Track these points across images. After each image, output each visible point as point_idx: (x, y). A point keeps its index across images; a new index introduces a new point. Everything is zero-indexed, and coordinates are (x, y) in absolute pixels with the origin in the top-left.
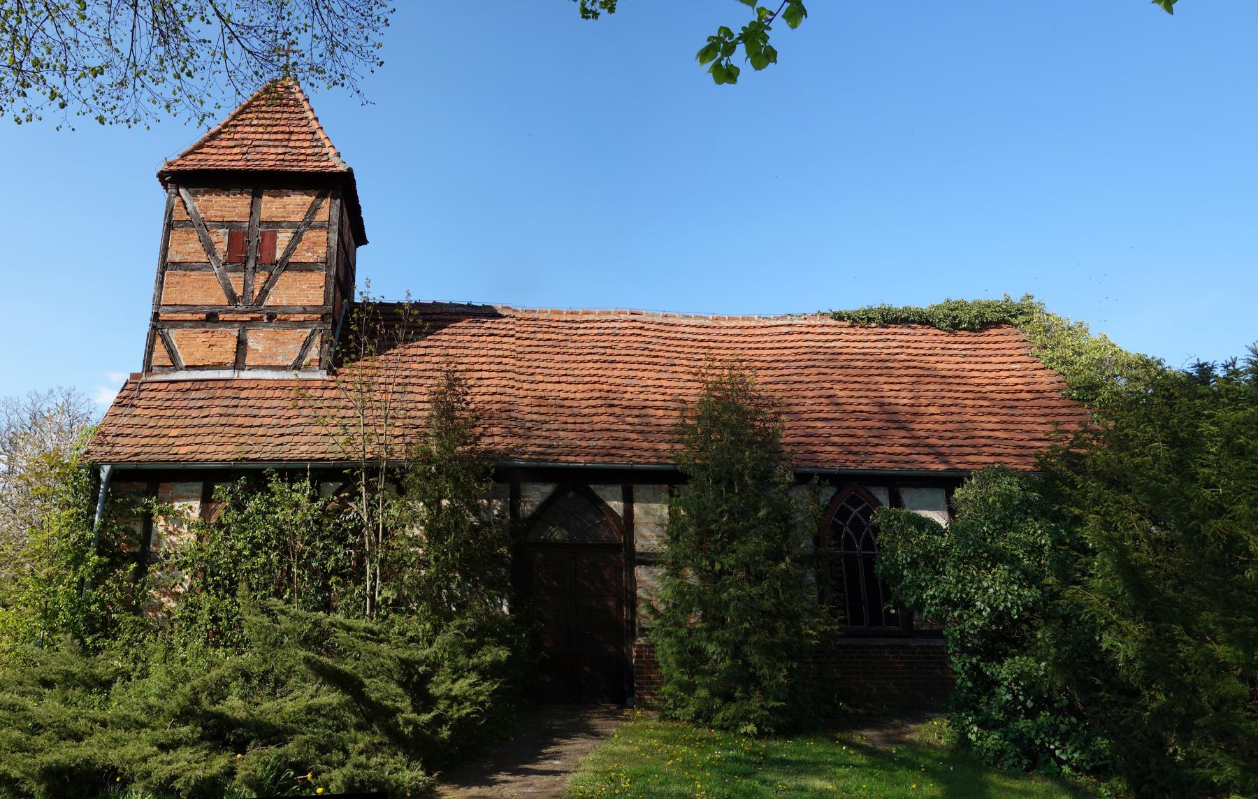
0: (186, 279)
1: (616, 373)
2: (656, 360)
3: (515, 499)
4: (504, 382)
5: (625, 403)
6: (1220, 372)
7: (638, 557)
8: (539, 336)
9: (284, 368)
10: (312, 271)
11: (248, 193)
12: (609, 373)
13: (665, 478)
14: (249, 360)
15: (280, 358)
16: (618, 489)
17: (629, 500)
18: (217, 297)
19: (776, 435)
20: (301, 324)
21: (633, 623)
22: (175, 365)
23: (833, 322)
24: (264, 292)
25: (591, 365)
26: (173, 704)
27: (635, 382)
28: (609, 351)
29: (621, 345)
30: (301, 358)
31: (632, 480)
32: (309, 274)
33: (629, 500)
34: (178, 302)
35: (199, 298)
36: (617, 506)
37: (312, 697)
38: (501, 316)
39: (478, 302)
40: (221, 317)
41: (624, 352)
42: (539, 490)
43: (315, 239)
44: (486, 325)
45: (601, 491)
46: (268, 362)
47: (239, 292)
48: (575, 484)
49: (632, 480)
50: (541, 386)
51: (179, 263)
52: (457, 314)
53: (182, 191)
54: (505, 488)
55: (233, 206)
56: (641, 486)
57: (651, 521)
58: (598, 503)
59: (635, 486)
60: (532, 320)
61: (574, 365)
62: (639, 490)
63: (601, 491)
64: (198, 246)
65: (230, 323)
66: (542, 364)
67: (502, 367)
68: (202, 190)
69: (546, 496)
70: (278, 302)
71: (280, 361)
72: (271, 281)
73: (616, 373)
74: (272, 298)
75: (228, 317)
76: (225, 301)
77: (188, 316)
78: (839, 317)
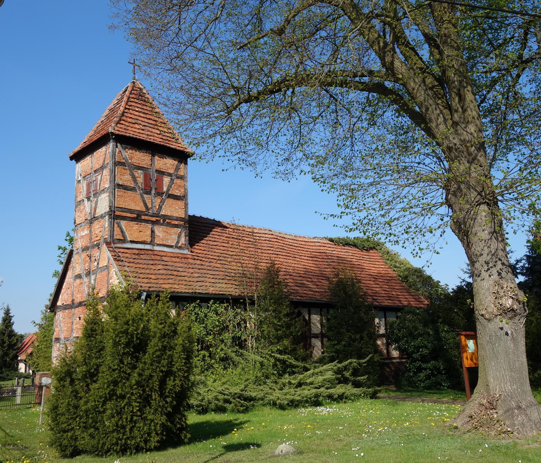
0: (126, 194)
6: (268, 174)
9: (171, 247)
10: (179, 200)
11: (149, 153)
14: (157, 241)
15: (169, 241)
16: (307, 309)
18: (140, 207)
19: (112, 296)
20: (176, 226)
22: (124, 241)
23: (330, 242)
24: (160, 207)
30: (178, 242)
32: (178, 201)
34: (124, 207)
35: (133, 207)
37: (242, 391)
38: (227, 228)
40: (143, 217)
43: (179, 184)
46: (165, 243)
47: (150, 206)
51: (121, 185)
53: (118, 145)
55: (141, 158)
60: (237, 229)
62: (313, 310)
64: (129, 177)
65: (147, 221)
68: (129, 147)
70: (166, 213)
71: (169, 243)
72: (163, 202)
74: (164, 211)
75: (146, 218)
76: (144, 209)
77: (129, 215)
78: (331, 240)
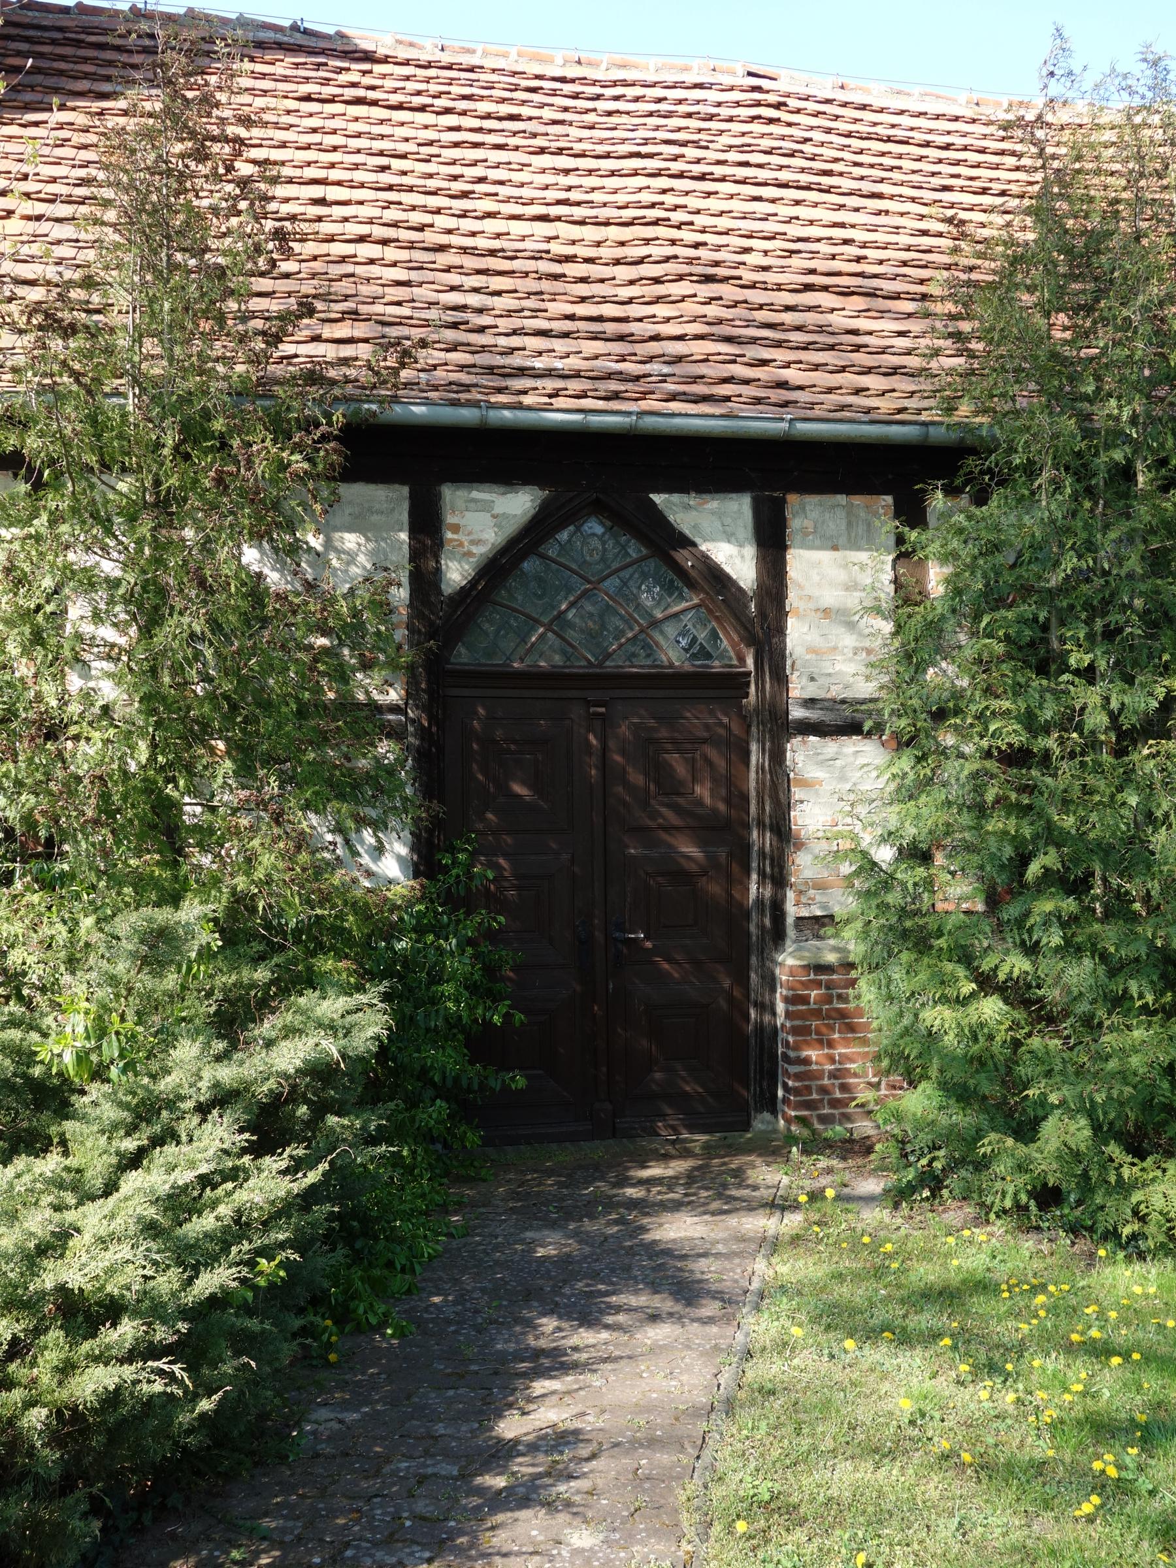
1: (714, 204)
2: (826, 181)
3: (427, 528)
4: (392, 214)
5: (748, 276)
7: (797, 713)
8: (484, 107)
12: (693, 202)
13: (894, 472)
17: (772, 542)
21: (777, 909)
25: (641, 181)
26: (265, 1088)
27: (771, 227)
28: (691, 152)
29: (725, 140)
31: (779, 472)
33: (772, 542)
36: (738, 561)
39: (323, 21)
41: (733, 156)
42: (487, 507)
44: (344, 78)
45: (685, 512)
48: (610, 477)
49: (779, 472)
50: (491, 226)
52: (260, 45)
54: (391, 500)
56: (812, 500)
57: (840, 601)
58: (666, 543)
59: (793, 499)
61: (593, 181)
62: (806, 512)
63: (685, 512)
66: (494, 174)
67: (386, 178)
69: (511, 529)
73: (714, 204)
